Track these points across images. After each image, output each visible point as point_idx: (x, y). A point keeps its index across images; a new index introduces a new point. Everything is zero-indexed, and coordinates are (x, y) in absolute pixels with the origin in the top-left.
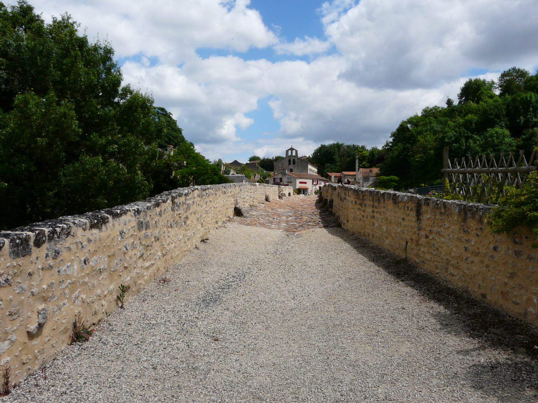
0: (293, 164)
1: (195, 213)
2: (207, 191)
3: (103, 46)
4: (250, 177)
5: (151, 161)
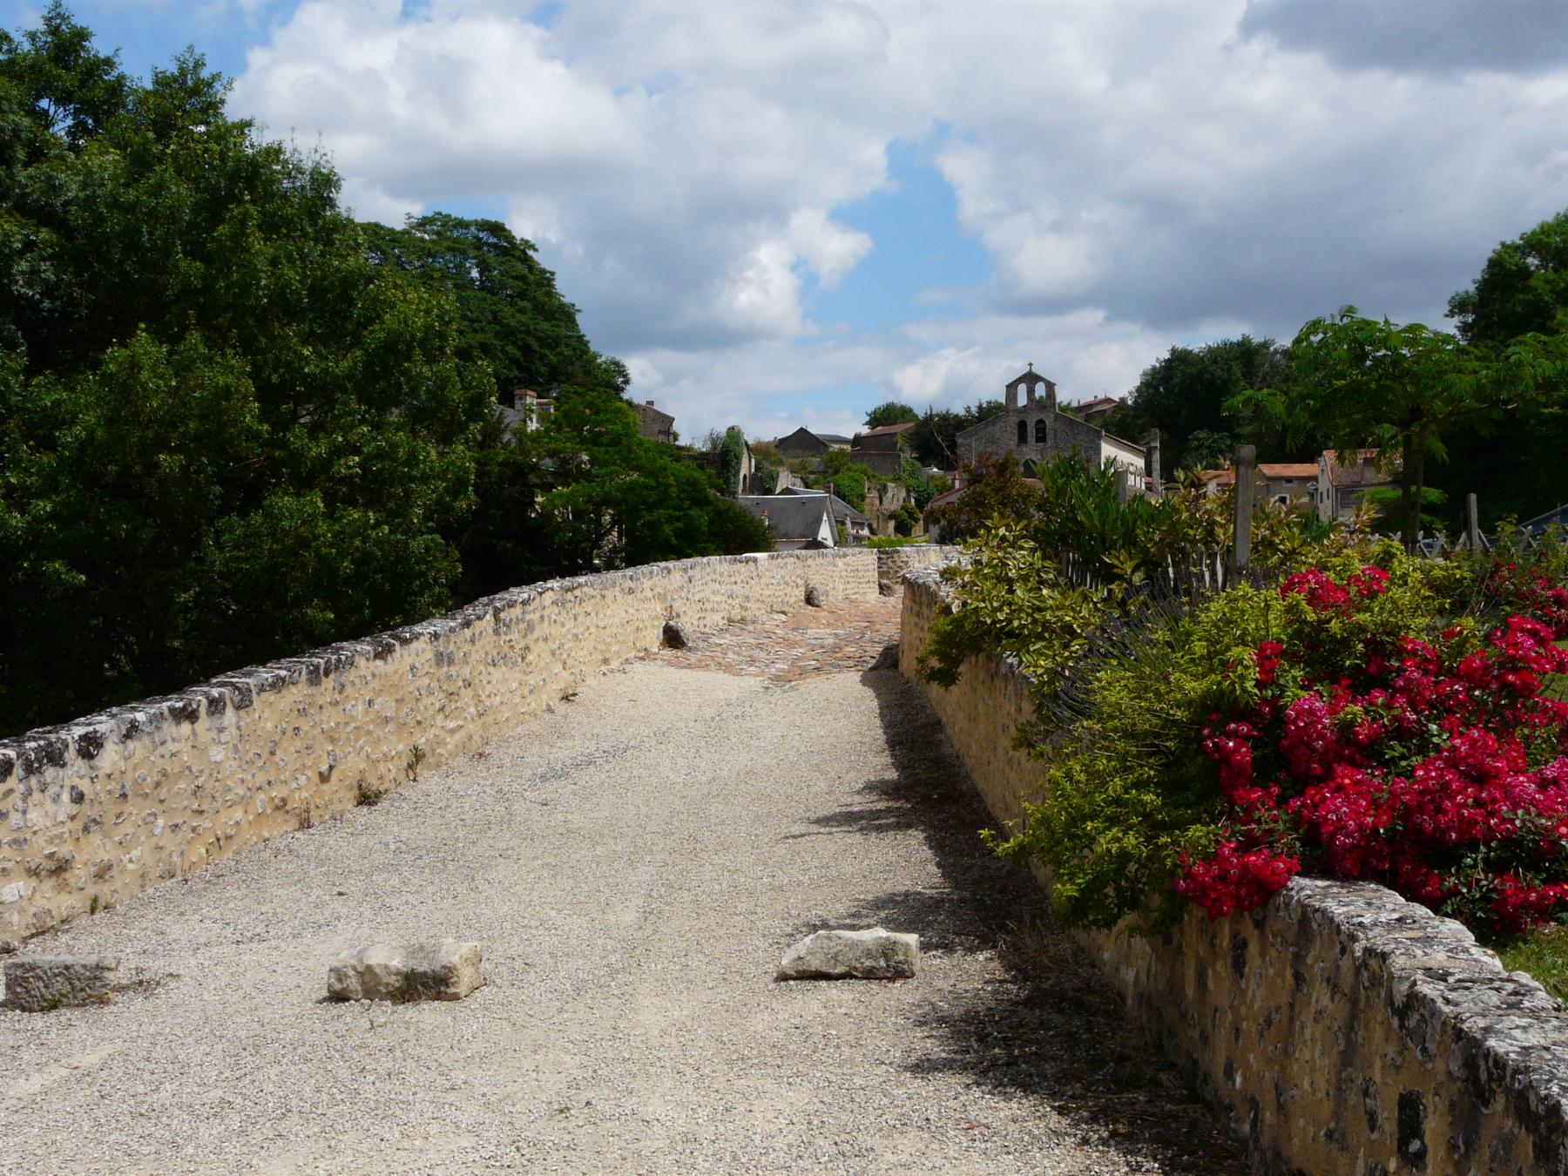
0: (1038, 440)
1: (546, 640)
2: (577, 592)
3: (308, 165)
4: (862, 497)
5: (455, 499)
